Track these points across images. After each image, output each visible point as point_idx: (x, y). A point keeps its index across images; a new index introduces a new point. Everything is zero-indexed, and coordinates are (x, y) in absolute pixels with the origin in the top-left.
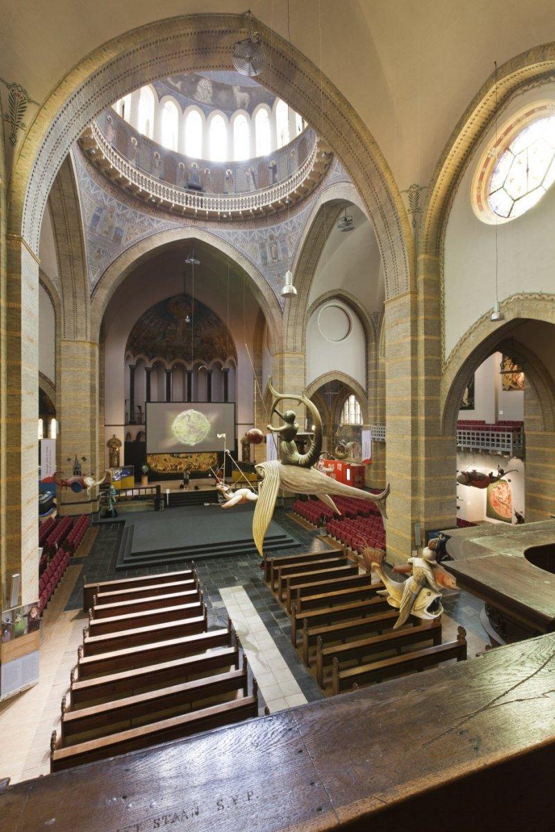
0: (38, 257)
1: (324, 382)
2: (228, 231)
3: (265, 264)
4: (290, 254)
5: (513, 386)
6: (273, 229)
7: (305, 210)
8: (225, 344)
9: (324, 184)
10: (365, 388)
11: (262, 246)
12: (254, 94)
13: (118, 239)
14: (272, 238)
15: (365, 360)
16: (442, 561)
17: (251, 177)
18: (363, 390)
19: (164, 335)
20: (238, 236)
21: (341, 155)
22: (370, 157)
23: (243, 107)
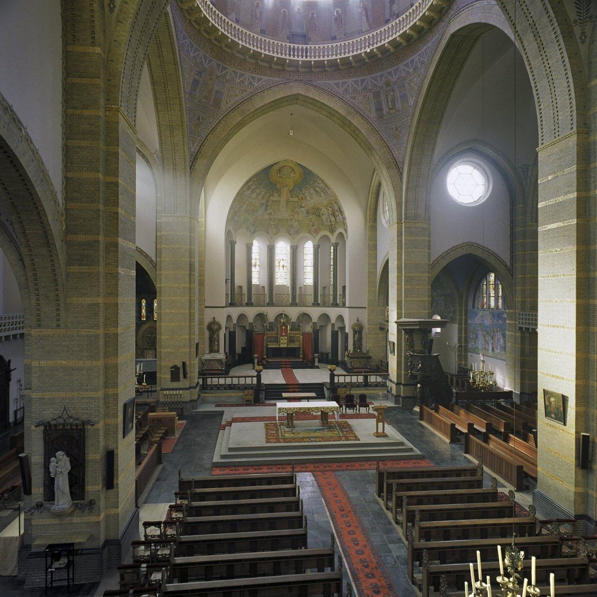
1: (453, 256)
3: (380, 117)
4: (411, 101)
6: (389, 73)
7: (430, 44)
8: (334, 215)
9: (455, 7)
10: (509, 264)
11: (377, 95)
13: (217, 104)
14: (388, 84)
18: (506, 266)
19: (267, 206)
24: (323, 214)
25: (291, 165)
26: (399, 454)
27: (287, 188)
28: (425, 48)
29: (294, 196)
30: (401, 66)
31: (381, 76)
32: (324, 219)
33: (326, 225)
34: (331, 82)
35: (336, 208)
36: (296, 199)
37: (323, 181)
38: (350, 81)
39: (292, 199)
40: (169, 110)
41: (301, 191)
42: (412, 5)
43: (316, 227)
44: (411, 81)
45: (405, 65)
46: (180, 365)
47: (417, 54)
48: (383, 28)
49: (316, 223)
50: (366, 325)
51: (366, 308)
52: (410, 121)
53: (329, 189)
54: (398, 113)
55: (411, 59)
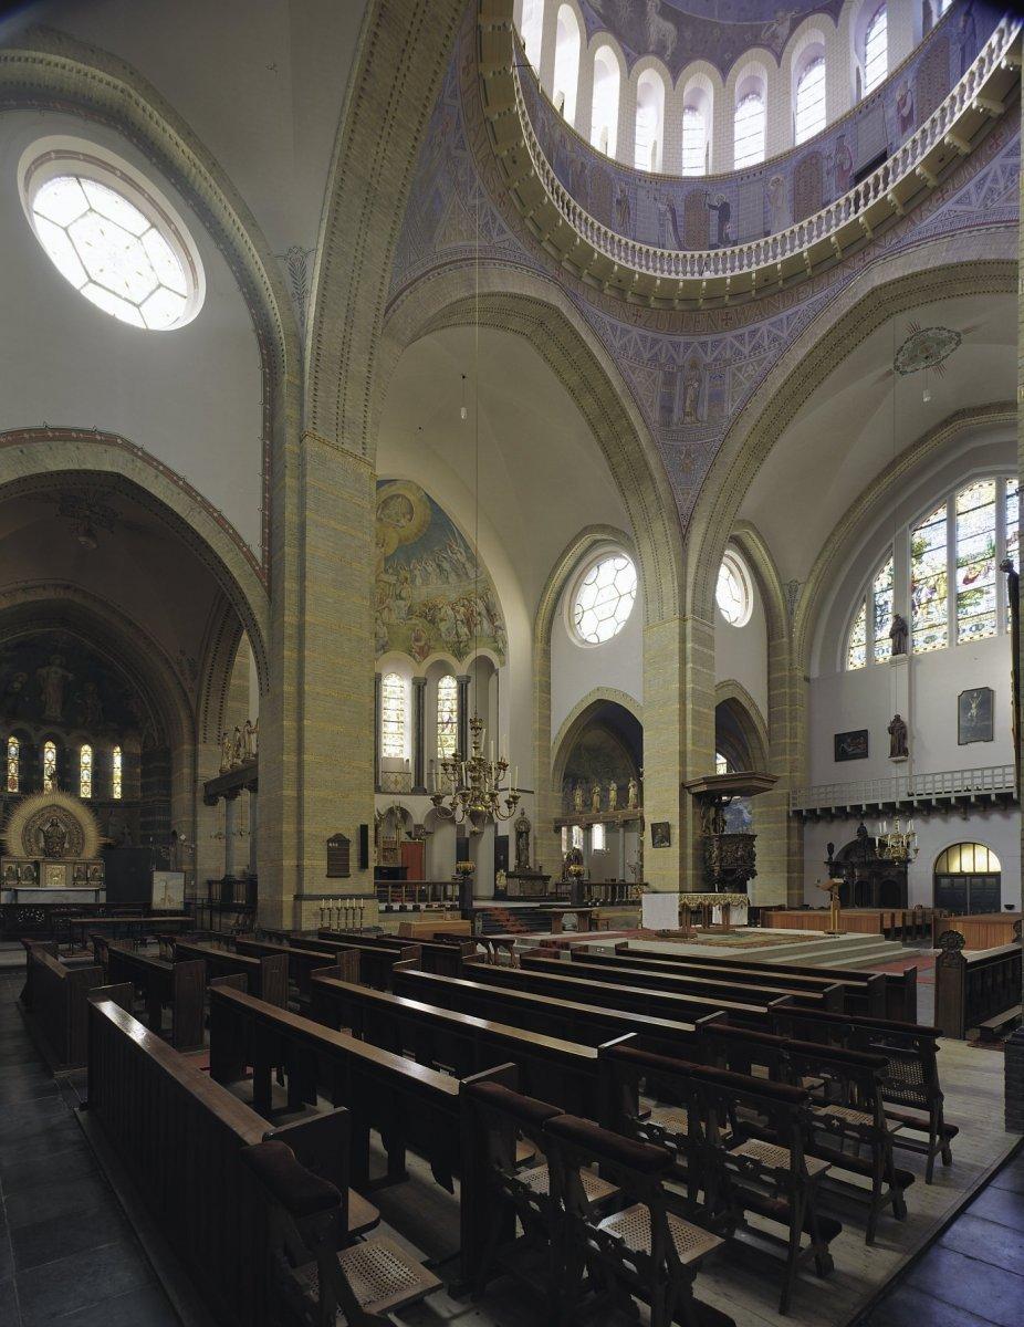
0: (935, 20)
1: (585, 706)
2: (613, 321)
3: (667, 423)
6: (704, 344)
7: (804, 306)
8: (468, 622)
11: (669, 381)
12: (688, 34)
15: (766, 670)
16: (822, 1085)
17: (669, 216)
20: (629, 341)
23: (660, 53)
24: (442, 620)
25: (412, 498)
26: (787, 976)
27: (383, 550)
28: (790, 312)
29: (391, 571)
30: (729, 337)
31: (687, 345)
32: (443, 629)
33: (447, 643)
34: (607, 319)
35: (481, 607)
36: (393, 579)
37: (467, 548)
38: (636, 332)
39: (385, 577)
40: (385, 134)
41: (409, 564)
42: (767, 234)
43: (422, 643)
44: (739, 369)
45: (736, 337)
46: (352, 835)
47: (767, 322)
48: (747, 245)
49: (424, 636)
50: (535, 825)
51: (532, 792)
52: (718, 444)
53: (476, 566)
54: (699, 425)
55: (752, 328)
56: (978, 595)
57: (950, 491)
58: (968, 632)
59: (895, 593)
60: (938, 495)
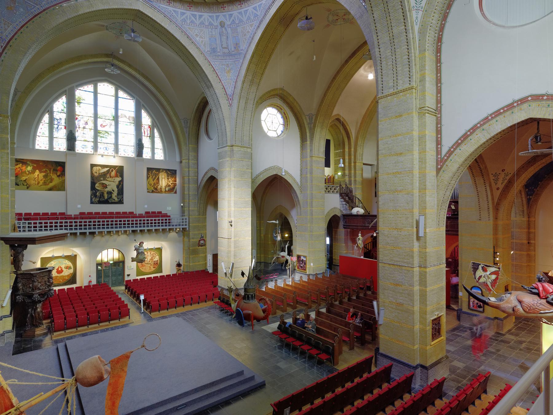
5: (154, 190)
21: (252, 61)
22: (261, 78)
56: (107, 134)
57: (157, 126)
58: (102, 149)
59: (264, 291)
60: (156, 120)
